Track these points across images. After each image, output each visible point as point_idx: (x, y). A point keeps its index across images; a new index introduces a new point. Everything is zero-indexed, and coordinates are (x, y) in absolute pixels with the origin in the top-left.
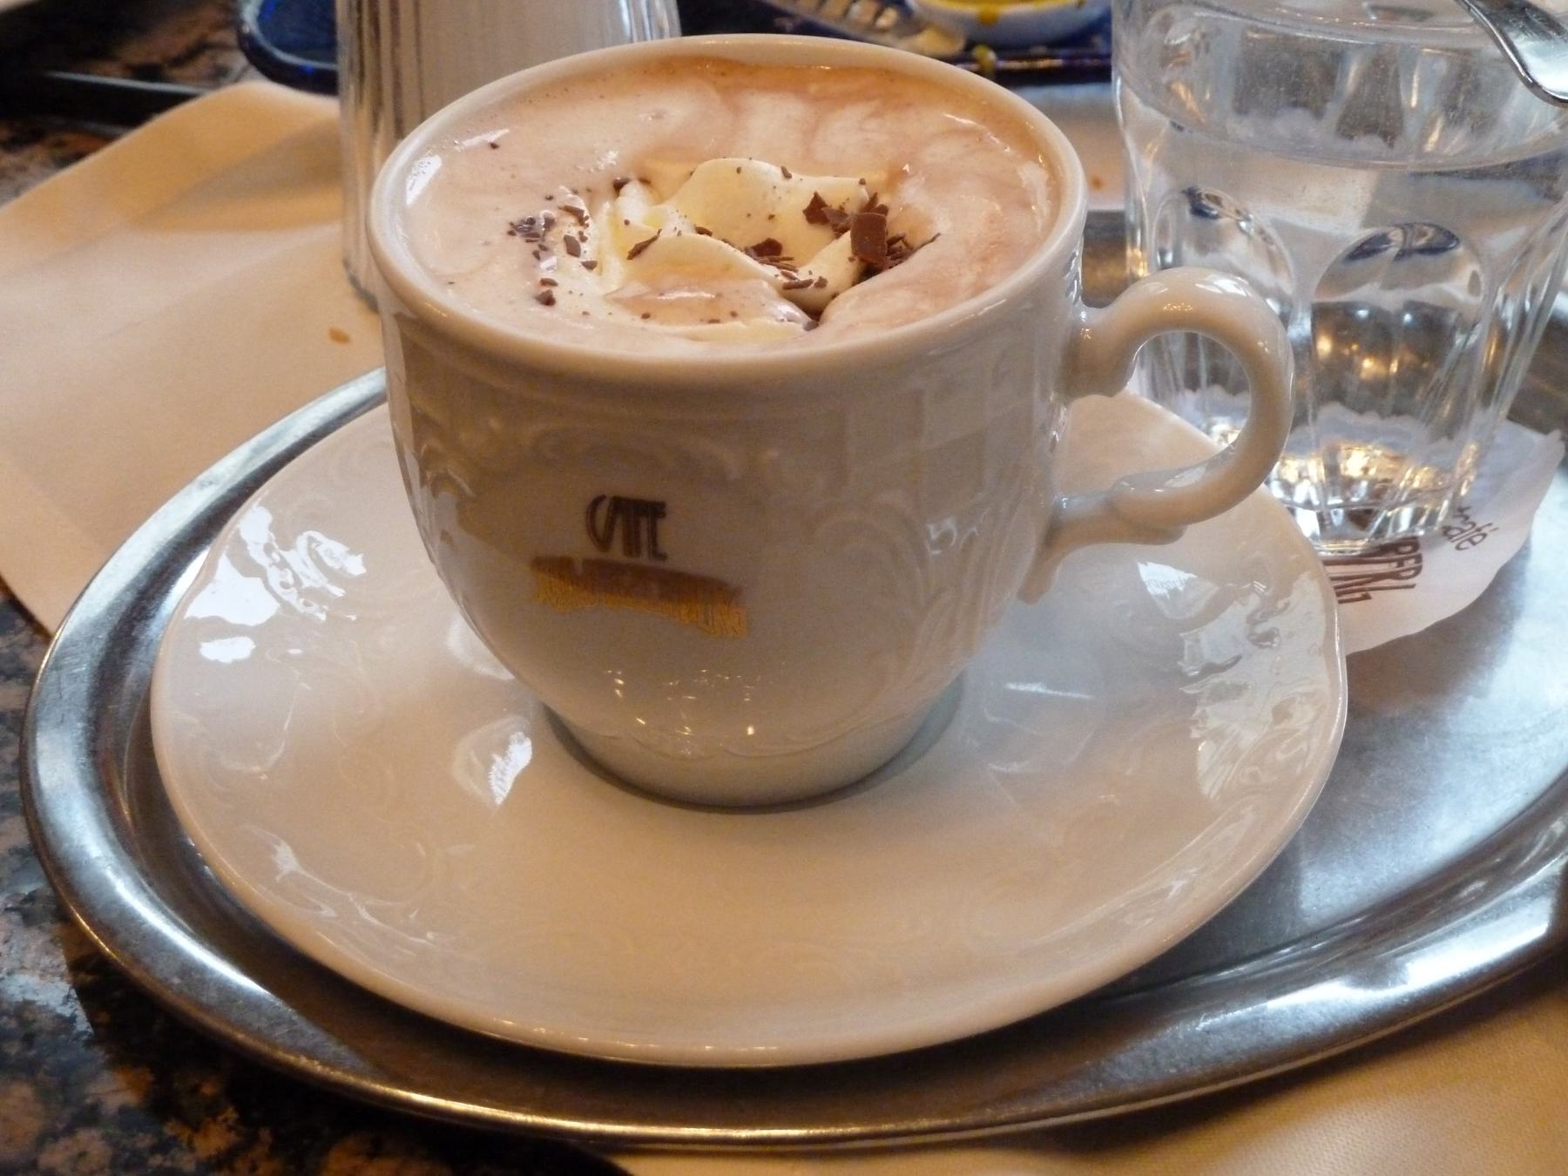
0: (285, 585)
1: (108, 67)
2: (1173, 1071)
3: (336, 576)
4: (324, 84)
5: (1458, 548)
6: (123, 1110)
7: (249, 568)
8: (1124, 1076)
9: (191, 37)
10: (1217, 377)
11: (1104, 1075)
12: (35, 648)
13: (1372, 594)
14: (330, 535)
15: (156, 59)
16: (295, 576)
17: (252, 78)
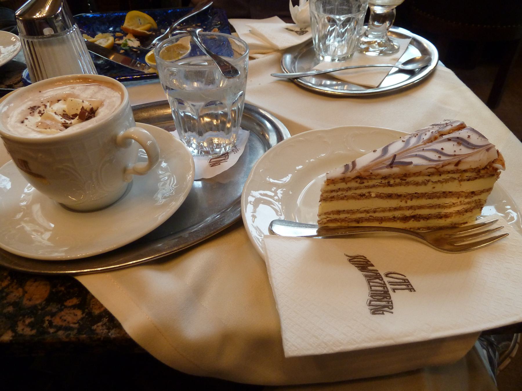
1: (2, 86)
5: (234, 153)
15: (12, 84)
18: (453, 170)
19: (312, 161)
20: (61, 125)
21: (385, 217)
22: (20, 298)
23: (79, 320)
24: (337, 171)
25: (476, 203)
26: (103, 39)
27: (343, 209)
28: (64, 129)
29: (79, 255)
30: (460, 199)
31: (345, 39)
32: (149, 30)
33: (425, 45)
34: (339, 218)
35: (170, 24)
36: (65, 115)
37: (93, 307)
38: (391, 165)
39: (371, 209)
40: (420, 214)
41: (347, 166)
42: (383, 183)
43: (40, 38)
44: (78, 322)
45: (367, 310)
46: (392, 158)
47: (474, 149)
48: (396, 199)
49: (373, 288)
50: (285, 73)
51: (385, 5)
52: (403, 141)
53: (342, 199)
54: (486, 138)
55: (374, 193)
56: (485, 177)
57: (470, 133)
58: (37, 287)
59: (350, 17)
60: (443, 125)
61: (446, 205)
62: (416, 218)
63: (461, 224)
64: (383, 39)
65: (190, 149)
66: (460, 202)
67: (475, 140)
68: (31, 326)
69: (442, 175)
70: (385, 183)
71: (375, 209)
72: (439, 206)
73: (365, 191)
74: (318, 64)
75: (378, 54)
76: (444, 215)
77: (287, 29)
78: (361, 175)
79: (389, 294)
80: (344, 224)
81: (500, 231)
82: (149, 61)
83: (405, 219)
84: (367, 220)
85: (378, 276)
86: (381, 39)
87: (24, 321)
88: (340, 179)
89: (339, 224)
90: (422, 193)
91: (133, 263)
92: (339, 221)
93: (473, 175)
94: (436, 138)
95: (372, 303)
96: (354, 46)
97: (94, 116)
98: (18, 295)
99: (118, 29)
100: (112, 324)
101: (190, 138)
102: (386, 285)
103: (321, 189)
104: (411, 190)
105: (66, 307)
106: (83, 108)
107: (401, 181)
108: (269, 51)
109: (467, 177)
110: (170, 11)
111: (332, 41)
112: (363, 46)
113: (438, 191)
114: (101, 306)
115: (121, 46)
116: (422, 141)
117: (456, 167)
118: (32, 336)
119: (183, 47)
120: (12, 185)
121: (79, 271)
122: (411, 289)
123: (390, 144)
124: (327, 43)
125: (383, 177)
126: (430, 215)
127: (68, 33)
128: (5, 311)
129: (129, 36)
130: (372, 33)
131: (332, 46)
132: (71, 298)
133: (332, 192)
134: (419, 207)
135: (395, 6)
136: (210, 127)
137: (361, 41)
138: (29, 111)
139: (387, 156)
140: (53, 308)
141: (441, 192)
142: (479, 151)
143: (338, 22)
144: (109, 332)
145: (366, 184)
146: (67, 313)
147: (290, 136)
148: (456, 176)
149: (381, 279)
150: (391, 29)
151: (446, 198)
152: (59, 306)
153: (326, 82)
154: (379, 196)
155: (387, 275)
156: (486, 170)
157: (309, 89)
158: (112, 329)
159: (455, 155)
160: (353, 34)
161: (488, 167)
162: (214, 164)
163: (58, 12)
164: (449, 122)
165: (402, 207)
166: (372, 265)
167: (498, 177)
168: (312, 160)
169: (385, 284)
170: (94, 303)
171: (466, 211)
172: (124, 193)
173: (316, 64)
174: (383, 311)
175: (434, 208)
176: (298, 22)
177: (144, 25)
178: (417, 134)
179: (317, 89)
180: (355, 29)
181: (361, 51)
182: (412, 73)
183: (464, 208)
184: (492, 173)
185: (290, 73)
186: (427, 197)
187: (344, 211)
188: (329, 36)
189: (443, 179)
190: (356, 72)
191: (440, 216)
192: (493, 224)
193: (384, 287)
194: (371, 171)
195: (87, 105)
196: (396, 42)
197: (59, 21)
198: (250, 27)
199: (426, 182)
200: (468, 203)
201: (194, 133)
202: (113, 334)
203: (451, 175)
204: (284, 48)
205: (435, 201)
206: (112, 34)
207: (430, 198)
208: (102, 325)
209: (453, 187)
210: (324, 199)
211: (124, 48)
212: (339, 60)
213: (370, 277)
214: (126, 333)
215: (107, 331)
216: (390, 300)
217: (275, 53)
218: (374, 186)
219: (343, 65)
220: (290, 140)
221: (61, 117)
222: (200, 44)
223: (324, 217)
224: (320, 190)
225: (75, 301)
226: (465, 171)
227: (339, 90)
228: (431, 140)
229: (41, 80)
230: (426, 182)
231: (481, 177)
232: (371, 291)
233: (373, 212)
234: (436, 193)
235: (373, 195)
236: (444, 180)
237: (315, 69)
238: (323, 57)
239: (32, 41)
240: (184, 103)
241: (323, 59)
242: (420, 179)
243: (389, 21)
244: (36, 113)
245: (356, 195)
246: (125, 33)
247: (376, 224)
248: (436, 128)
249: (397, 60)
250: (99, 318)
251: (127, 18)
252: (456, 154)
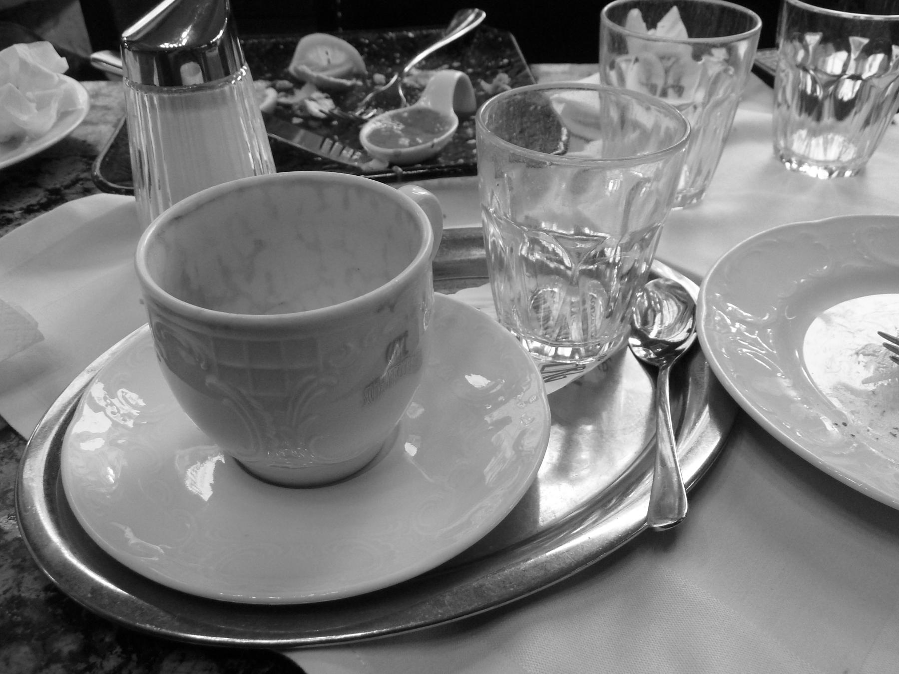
0: (113, 413)
2: (512, 589)
3: (135, 407)
4: (130, 192)
6: (71, 653)
7: (97, 408)
8: (493, 594)
9: (73, 176)
12: (21, 446)
14: (131, 391)
15: (58, 186)
16: (117, 409)
17: (99, 193)
32: (348, 75)
43: (176, 92)
246: (299, 82)
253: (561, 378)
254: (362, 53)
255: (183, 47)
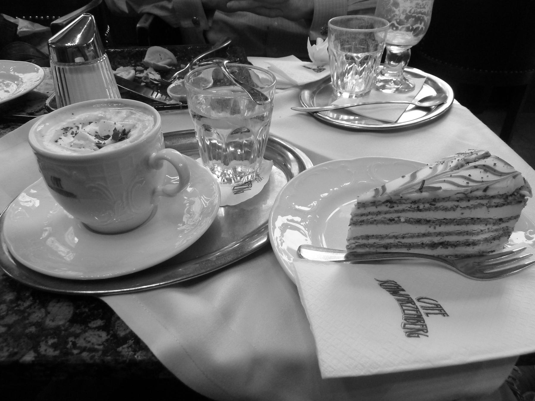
5: (258, 182)
10: (214, 158)
11: (14, 314)
13: (244, 191)
18: (482, 196)
19: (337, 190)
20: (94, 145)
21: (413, 243)
22: (42, 319)
23: (104, 342)
24: (368, 196)
25: (504, 230)
26: (125, 72)
27: (372, 234)
28: (98, 149)
29: (104, 276)
30: (488, 226)
31: (362, 77)
32: (169, 65)
33: (440, 85)
34: (368, 243)
35: (190, 60)
36: (97, 136)
37: (117, 329)
38: (421, 190)
39: (400, 234)
40: (448, 241)
41: (377, 190)
42: (413, 208)
43: (71, 65)
44: (103, 344)
45: (402, 333)
46: (421, 183)
47: (501, 176)
48: (424, 225)
49: (406, 312)
50: (304, 107)
51: (400, 45)
52: (430, 168)
53: (372, 223)
54: (512, 167)
55: (403, 217)
56: (513, 203)
57: (496, 162)
58: (60, 307)
59: (368, 55)
60: (469, 154)
61: (474, 231)
62: (444, 245)
63: (489, 252)
64: (399, 77)
65: (215, 176)
66: (488, 229)
67: (500, 167)
68: (54, 346)
69: (470, 201)
70: (415, 208)
71: (404, 234)
72: (467, 233)
73: (394, 216)
74: (335, 100)
75: (394, 91)
76: (471, 242)
77: (304, 66)
78: (391, 198)
79: (423, 318)
80: (372, 250)
81: (530, 259)
82: (171, 93)
83: (433, 246)
84: (396, 246)
85: (412, 302)
86: (397, 78)
87: (47, 342)
88: (370, 203)
89: (367, 250)
90: (450, 219)
91: (160, 285)
92: (368, 246)
93: (501, 201)
94: (462, 166)
95: (407, 326)
96: (371, 84)
97: (127, 138)
98: (40, 315)
99: (138, 64)
100: (138, 346)
101: (214, 166)
102: (418, 309)
103: (351, 213)
104: (440, 215)
105: (90, 328)
106: (115, 129)
107: (430, 206)
108: (287, 87)
109: (495, 203)
110: (190, 48)
111: (350, 78)
112: (379, 84)
113: (466, 217)
114: (127, 327)
115: (142, 79)
116: (449, 168)
117: (484, 193)
118: (55, 357)
119: (206, 81)
120: (40, 203)
121: (106, 291)
122: (445, 314)
123: (418, 171)
124: (345, 80)
125: (412, 202)
126: (458, 242)
127: (99, 62)
128: (27, 331)
129: (150, 70)
130: (389, 72)
131: (349, 83)
132: (95, 319)
133: (363, 216)
134: (447, 233)
135: (411, 47)
136: (235, 156)
137: (377, 79)
138: (63, 131)
139: (417, 180)
140: (77, 329)
141: (469, 218)
142: (507, 178)
143: (356, 59)
144: (135, 354)
145: (396, 208)
146: (91, 335)
147: (313, 166)
148: (484, 202)
149: (413, 303)
150: (406, 69)
151: (474, 224)
152: (83, 327)
153: (344, 117)
154: (408, 221)
155: (419, 300)
156: (513, 196)
157: (328, 122)
158: (138, 352)
159: (483, 181)
160: (371, 72)
161: (516, 194)
162: (238, 191)
163: (89, 42)
164: (474, 151)
165: (431, 233)
166: (403, 290)
167: (525, 205)
168: (336, 189)
169: (417, 308)
170: (118, 325)
171: (494, 239)
172: (143, 223)
173: (334, 100)
174: (418, 334)
175: (463, 235)
176: (315, 61)
177: (164, 60)
178: (443, 161)
179: (337, 123)
180: (372, 67)
181: (378, 89)
182: (428, 110)
183: (491, 236)
184: (520, 200)
185: (309, 107)
186: (455, 223)
187: (373, 236)
188: (347, 74)
189: (472, 205)
190: (374, 108)
191: (468, 244)
192: (521, 252)
193: (417, 311)
194: (401, 195)
195: (119, 126)
196: (412, 81)
197: (91, 51)
198: (269, 63)
199: (455, 207)
200: (496, 230)
201: (219, 161)
202: (139, 356)
203: (479, 201)
204: (303, 84)
205: (463, 228)
206: (133, 68)
207: (458, 225)
208: (128, 348)
209: (481, 213)
210: (354, 223)
211: (145, 81)
212: (356, 97)
213: (402, 301)
214: (153, 355)
215: (134, 353)
216: (424, 324)
217: (294, 88)
218: (403, 211)
219: (360, 101)
220: (311, 170)
221: (95, 138)
222: (228, 74)
223: (353, 241)
224: (350, 214)
225: (99, 323)
226: (493, 197)
227: (357, 125)
228: (458, 167)
229: (68, 105)
230: (455, 207)
231: (508, 204)
232: (405, 314)
233: (402, 238)
234: (464, 219)
235: (403, 220)
236: (472, 206)
237: (333, 105)
238: (340, 93)
239: (63, 68)
240: (211, 130)
241: (341, 95)
242: (449, 204)
243: (404, 61)
244: (69, 133)
245: (386, 219)
247: (404, 250)
248: (462, 157)
249: (414, 97)
250: (125, 340)
251: (148, 53)
252: (483, 180)
253: (242, 193)
254: (175, 55)
255: (76, 45)
